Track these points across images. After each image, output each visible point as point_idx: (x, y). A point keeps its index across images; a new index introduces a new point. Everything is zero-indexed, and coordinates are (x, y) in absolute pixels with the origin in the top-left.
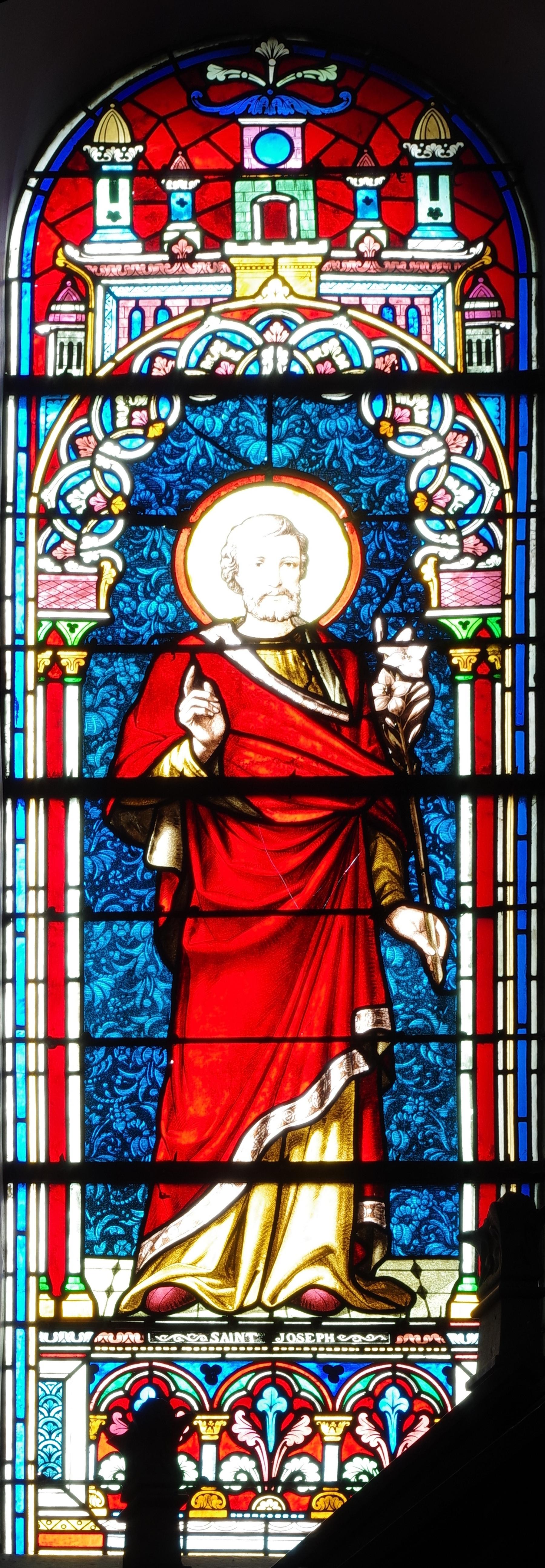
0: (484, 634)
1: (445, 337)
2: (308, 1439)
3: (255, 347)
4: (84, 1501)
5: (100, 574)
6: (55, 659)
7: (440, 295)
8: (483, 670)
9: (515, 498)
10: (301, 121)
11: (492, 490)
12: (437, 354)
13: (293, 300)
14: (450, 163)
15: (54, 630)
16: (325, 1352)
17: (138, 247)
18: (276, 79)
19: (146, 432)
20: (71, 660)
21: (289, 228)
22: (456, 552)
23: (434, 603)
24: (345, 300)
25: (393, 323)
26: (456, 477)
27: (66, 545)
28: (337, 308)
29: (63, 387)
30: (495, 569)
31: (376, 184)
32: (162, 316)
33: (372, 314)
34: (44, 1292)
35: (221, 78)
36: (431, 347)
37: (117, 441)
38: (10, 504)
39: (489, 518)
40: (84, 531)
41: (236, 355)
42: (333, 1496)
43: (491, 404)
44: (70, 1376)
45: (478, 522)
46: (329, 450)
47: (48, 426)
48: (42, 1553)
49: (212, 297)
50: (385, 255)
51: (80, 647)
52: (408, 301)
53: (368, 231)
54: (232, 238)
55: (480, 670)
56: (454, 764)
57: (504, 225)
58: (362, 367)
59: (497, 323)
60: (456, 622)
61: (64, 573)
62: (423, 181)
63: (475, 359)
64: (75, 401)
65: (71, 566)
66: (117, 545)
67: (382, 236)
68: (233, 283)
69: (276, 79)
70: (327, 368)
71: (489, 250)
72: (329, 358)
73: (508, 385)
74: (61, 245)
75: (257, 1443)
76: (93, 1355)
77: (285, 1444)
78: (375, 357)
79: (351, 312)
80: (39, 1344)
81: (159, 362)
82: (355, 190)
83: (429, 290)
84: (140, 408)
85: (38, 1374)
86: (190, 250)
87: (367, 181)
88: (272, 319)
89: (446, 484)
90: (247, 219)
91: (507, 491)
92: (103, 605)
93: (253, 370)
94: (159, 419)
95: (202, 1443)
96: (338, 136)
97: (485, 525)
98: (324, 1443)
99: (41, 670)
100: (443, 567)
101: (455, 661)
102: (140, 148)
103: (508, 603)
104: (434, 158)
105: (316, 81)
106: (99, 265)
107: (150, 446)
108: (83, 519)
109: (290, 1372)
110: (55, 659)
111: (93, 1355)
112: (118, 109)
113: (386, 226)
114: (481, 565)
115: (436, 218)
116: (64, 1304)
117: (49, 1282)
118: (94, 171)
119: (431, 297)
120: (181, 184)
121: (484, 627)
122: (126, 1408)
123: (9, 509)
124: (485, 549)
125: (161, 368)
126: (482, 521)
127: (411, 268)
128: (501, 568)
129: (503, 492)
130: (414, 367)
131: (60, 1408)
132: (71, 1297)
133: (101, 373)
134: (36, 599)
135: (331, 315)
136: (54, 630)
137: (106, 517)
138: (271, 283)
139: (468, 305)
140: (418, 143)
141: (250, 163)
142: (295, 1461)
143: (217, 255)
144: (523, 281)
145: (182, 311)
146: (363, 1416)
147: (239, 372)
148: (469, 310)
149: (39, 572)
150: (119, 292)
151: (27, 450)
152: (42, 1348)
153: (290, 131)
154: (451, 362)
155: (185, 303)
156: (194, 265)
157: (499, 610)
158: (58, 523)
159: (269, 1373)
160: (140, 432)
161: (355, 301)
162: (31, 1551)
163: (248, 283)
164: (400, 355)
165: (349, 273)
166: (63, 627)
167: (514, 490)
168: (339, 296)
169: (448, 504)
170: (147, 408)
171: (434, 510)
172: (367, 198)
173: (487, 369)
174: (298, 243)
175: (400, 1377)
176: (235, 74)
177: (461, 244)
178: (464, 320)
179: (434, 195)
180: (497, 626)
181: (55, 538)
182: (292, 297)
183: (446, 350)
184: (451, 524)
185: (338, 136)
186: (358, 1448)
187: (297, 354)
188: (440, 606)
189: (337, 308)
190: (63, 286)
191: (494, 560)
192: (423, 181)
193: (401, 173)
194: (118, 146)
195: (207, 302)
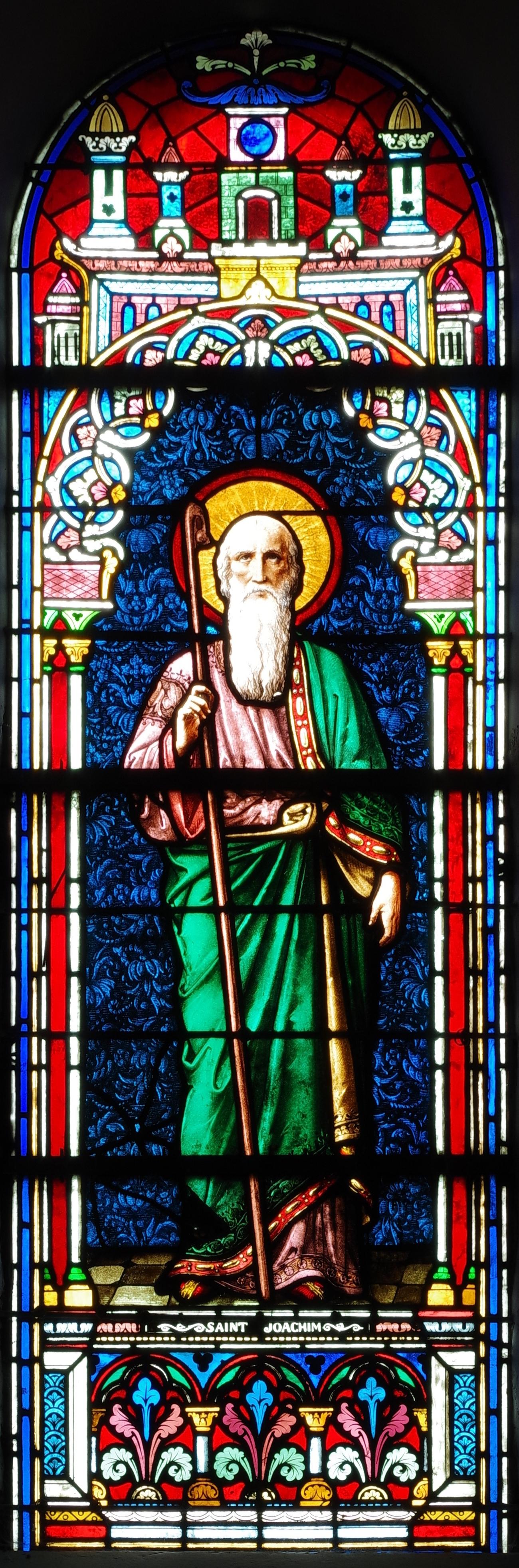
2: (180, 1429)
3: (238, 341)
4: (86, 1491)
5: (102, 563)
6: (60, 648)
7: (413, 290)
8: (456, 662)
11: (464, 484)
12: (411, 348)
13: (275, 301)
17: (131, 242)
18: (262, 66)
20: (76, 648)
23: (412, 595)
24: (322, 300)
25: (368, 320)
26: (431, 471)
28: (316, 308)
29: (63, 378)
32: (154, 312)
33: (348, 312)
36: (405, 341)
37: (116, 429)
39: (462, 511)
42: (320, 1486)
46: (312, 443)
47: (51, 416)
49: (199, 297)
50: (361, 254)
52: (382, 298)
53: (345, 230)
56: (429, 759)
57: (472, 218)
58: (339, 358)
59: (464, 316)
61: (69, 562)
64: (73, 393)
65: (75, 555)
66: (119, 533)
67: (185, 235)
68: (218, 284)
69: (262, 66)
72: (307, 351)
73: (480, 377)
74: (59, 237)
75: (246, 1433)
79: (329, 311)
80: (44, 1335)
83: (402, 286)
84: (136, 397)
85: (42, 1366)
87: (345, 174)
88: (254, 318)
89: (422, 478)
92: (105, 595)
93: (237, 360)
96: (319, 127)
97: (458, 519)
99: (46, 659)
102: (133, 138)
104: (408, 149)
106: (93, 259)
107: (147, 436)
110: (60, 648)
112: (111, 101)
114: (455, 559)
115: (408, 212)
116: (67, 1293)
117: (52, 1272)
119: (404, 293)
120: (171, 175)
125: (152, 358)
126: (456, 514)
128: (473, 562)
129: (474, 485)
133: (95, 364)
134: (41, 589)
138: (254, 284)
139: (440, 298)
140: (392, 132)
141: (236, 154)
142: (284, 1451)
143: (204, 256)
145: (171, 308)
148: (441, 303)
149: (45, 561)
150: (114, 287)
151: (30, 434)
153: (273, 121)
161: (332, 300)
165: (325, 273)
166: (68, 616)
168: (317, 296)
169: (425, 498)
172: (345, 192)
174: (278, 245)
176: (221, 64)
178: (436, 314)
181: (60, 527)
183: (419, 343)
184: (427, 516)
185: (319, 127)
188: (417, 599)
191: (466, 555)
194: (113, 135)
195: (195, 300)
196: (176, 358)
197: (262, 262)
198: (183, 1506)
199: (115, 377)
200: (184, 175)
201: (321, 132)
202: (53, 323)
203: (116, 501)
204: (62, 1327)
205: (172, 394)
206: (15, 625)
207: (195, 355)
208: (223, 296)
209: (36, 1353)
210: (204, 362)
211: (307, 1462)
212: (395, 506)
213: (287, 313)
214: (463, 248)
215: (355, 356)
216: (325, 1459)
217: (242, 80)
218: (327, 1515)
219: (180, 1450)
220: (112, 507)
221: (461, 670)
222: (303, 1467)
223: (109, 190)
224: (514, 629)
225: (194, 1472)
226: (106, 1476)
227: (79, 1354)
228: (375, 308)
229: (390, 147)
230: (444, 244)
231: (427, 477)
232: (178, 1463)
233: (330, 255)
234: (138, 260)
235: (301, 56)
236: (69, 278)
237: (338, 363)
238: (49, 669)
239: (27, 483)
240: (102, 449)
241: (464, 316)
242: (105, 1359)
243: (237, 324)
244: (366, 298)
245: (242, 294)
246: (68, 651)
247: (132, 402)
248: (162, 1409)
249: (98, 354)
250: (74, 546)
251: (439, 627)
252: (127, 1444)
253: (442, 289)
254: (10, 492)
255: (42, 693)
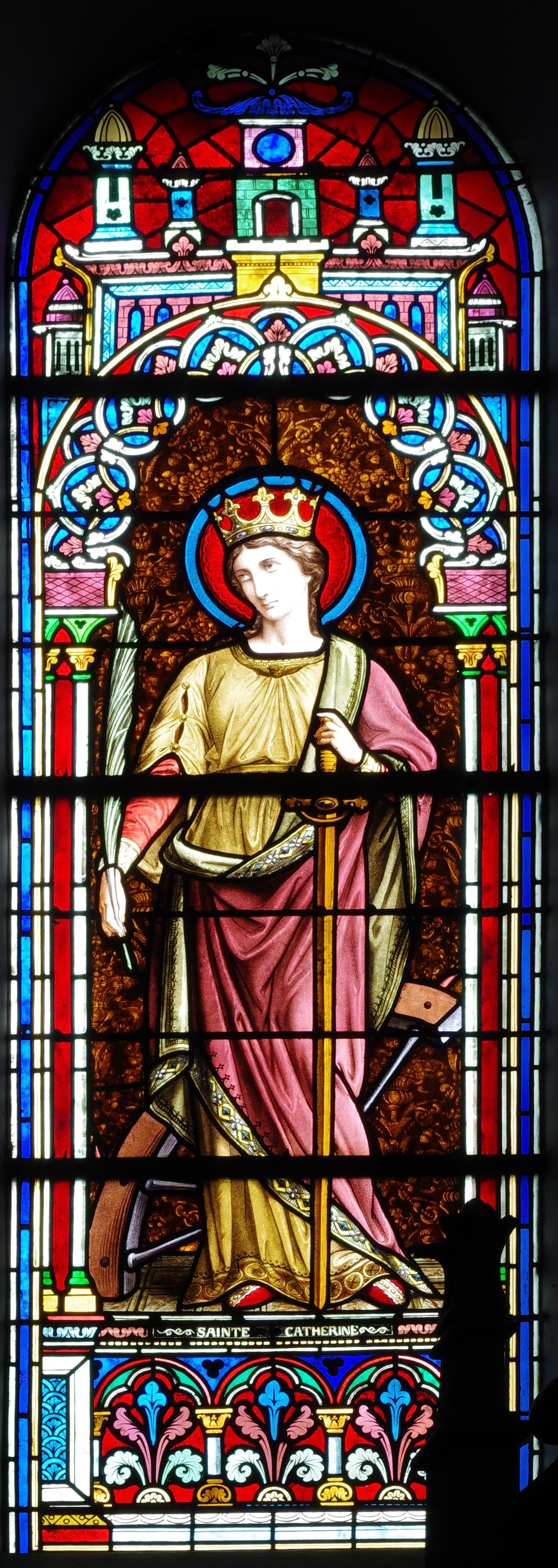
0: (490, 631)
1: (457, 335)
3: (257, 347)
4: (88, 1494)
5: (108, 571)
8: (489, 666)
9: (518, 494)
10: (301, 122)
11: (495, 489)
12: (440, 353)
13: (296, 298)
14: (451, 163)
15: (62, 627)
16: (330, 1345)
17: (138, 244)
18: (279, 76)
19: (151, 430)
21: (291, 226)
22: (461, 549)
23: (441, 600)
24: (347, 297)
25: (396, 320)
26: (462, 476)
27: (73, 540)
28: (338, 306)
30: (499, 567)
31: (378, 184)
33: (374, 311)
34: (47, 1287)
35: (221, 77)
36: (434, 346)
38: (15, 502)
40: (90, 527)
41: (237, 354)
42: (339, 1487)
43: (493, 403)
44: (73, 1371)
45: (480, 524)
48: (47, 1548)
49: (213, 295)
50: (388, 252)
51: (89, 644)
54: (234, 235)
55: (485, 667)
57: (506, 225)
58: (363, 366)
60: (462, 618)
61: (72, 569)
62: (426, 181)
63: (477, 359)
65: (79, 562)
67: (197, 235)
68: (234, 280)
70: (328, 367)
71: (492, 249)
73: (512, 385)
74: (62, 243)
76: (97, 1351)
77: (167, 1438)
78: (377, 356)
79: (353, 309)
80: (42, 1338)
81: (161, 360)
82: (170, 190)
84: (146, 407)
85: (41, 1371)
86: (191, 247)
90: (250, 219)
91: (510, 489)
92: (111, 600)
93: (256, 370)
94: (164, 418)
95: (327, 1435)
96: (339, 136)
97: (489, 525)
98: (327, 1435)
99: (48, 669)
100: (447, 564)
101: (460, 657)
102: (141, 148)
103: (513, 600)
104: (436, 157)
105: (319, 79)
108: (89, 515)
109: (291, 1366)
110: (63, 657)
111: (97, 1351)
113: (200, 226)
114: (485, 563)
115: (114, 219)
117: (52, 1277)
118: (96, 170)
119: (435, 294)
121: (490, 624)
122: (130, 1403)
123: (15, 508)
124: (489, 547)
125: (163, 365)
127: (412, 265)
128: (506, 566)
129: (506, 490)
130: (415, 366)
131: (63, 1404)
132: (73, 1291)
133: (103, 373)
135: (334, 313)
136: (62, 627)
137: (110, 515)
139: (471, 302)
140: (420, 142)
141: (251, 162)
144: (525, 281)
145: (183, 309)
146: (363, 1409)
147: (242, 371)
149: (46, 570)
152: (46, 1344)
153: (291, 132)
154: (454, 362)
155: (187, 301)
156: (195, 262)
157: (504, 608)
158: (64, 520)
159: (391, 1366)
160: (145, 429)
161: (357, 298)
162: (35, 1548)
163: (247, 282)
164: (400, 355)
166: (70, 623)
167: (516, 488)
168: (342, 293)
169: (454, 502)
170: (152, 406)
171: (438, 508)
173: (492, 369)
174: (299, 241)
175: (160, 1371)
176: (235, 73)
177: (464, 241)
178: (467, 318)
179: (437, 193)
180: (503, 622)
181: (63, 534)
182: (295, 294)
184: (456, 523)
186: (120, 1444)
187: (298, 353)
188: (446, 603)
189: (338, 306)
190: (60, 285)
191: (499, 559)
192: (426, 181)
193: (404, 173)
194: (120, 144)
195: (209, 299)
196: (189, 368)
197: (282, 257)
198: (193, 1508)
199: (123, 384)
200: (194, 182)
201: (342, 141)
202: (54, 332)
203: (122, 507)
204: (62, 1332)
205: (182, 403)
206: (15, 637)
207: (208, 365)
208: (239, 293)
209: (35, 1358)
210: (220, 372)
211: (325, 1463)
212: (421, 511)
213: (310, 312)
214: (496, 254)
215: (380, 365)
216: (344, 1460)
217: (260, 91)
218: (347, 1516)
219: (187, 1452)
220: (119, 514)
221: (494, 673)
222: (322, 1468)
223: (114, 196)
224: (552, 625)
225: (205, 1475)
226: (109, 1480)
227: (83, 1358)
228: (404, 308)
229: (417, 155)
230: (478, 248)
231: (457, 482)
232: (187, 1465)
233: (354, 251)
234: (147, 261)
235: (325, 63)
236: (71, 284)
237: (363, 371)
238: (50, 678)
239: (26, 493)
240: (106, 457)
241: (499, 322)
242: (107, 1366)
243: (256, 325)
244: (141, 302)
245: (261, 290)
246: (73, 660)
247: (140, 413)
248: (171, 1411)
249: (103, 365)
250: (78, 554)
251: (470, 631)
252: (131, 1447)
253: (475, 292)
254: (10, 502)
255: (44, 702)
